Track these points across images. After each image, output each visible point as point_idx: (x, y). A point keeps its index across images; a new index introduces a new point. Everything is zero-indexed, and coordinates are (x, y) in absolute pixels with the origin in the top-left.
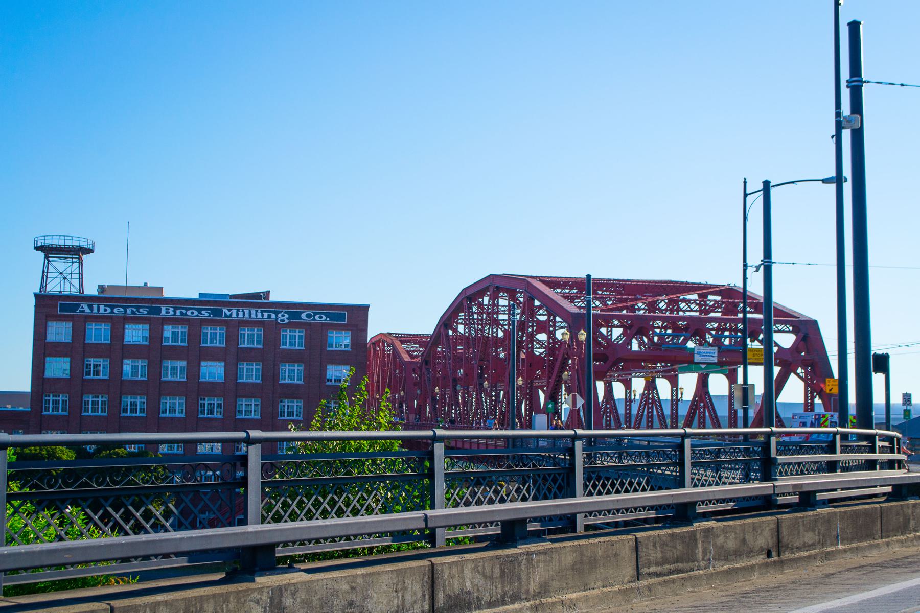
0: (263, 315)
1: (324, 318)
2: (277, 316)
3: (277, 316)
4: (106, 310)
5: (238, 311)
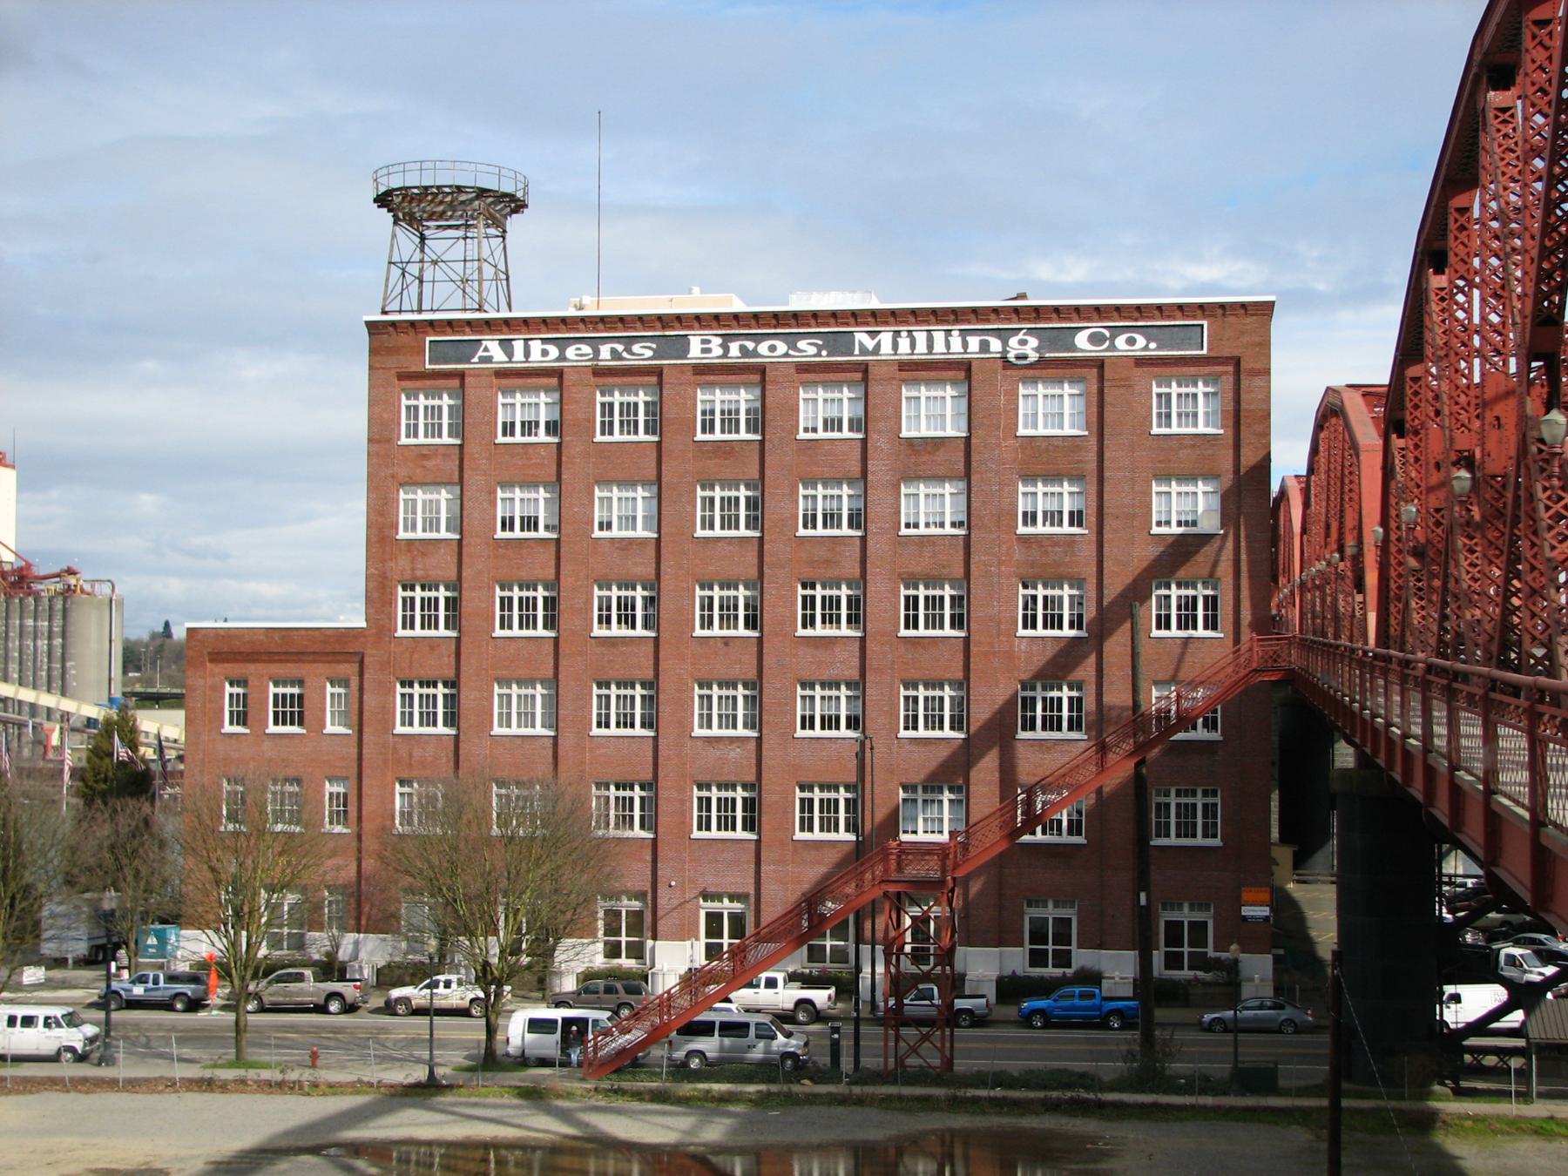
0: (965, 345)
1: (1141, 341)
2: (1005, 343)
3: (1005, 343)
4: (545, 353)
5: (897, 333)
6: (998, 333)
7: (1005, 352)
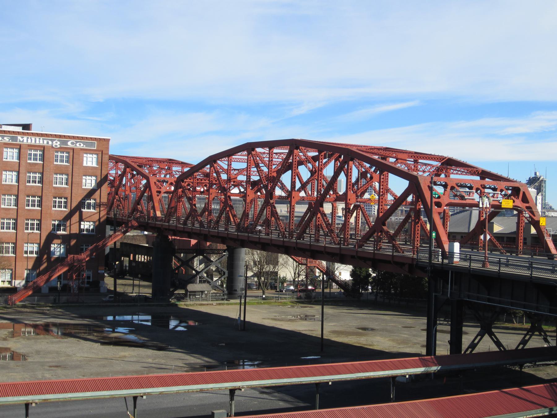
0: (43, 142)
1: (82, 145)
2: (52, 142)
3: (52, 142)
5: (40, 139)
6: (51, 140)
7: (52, 145)
